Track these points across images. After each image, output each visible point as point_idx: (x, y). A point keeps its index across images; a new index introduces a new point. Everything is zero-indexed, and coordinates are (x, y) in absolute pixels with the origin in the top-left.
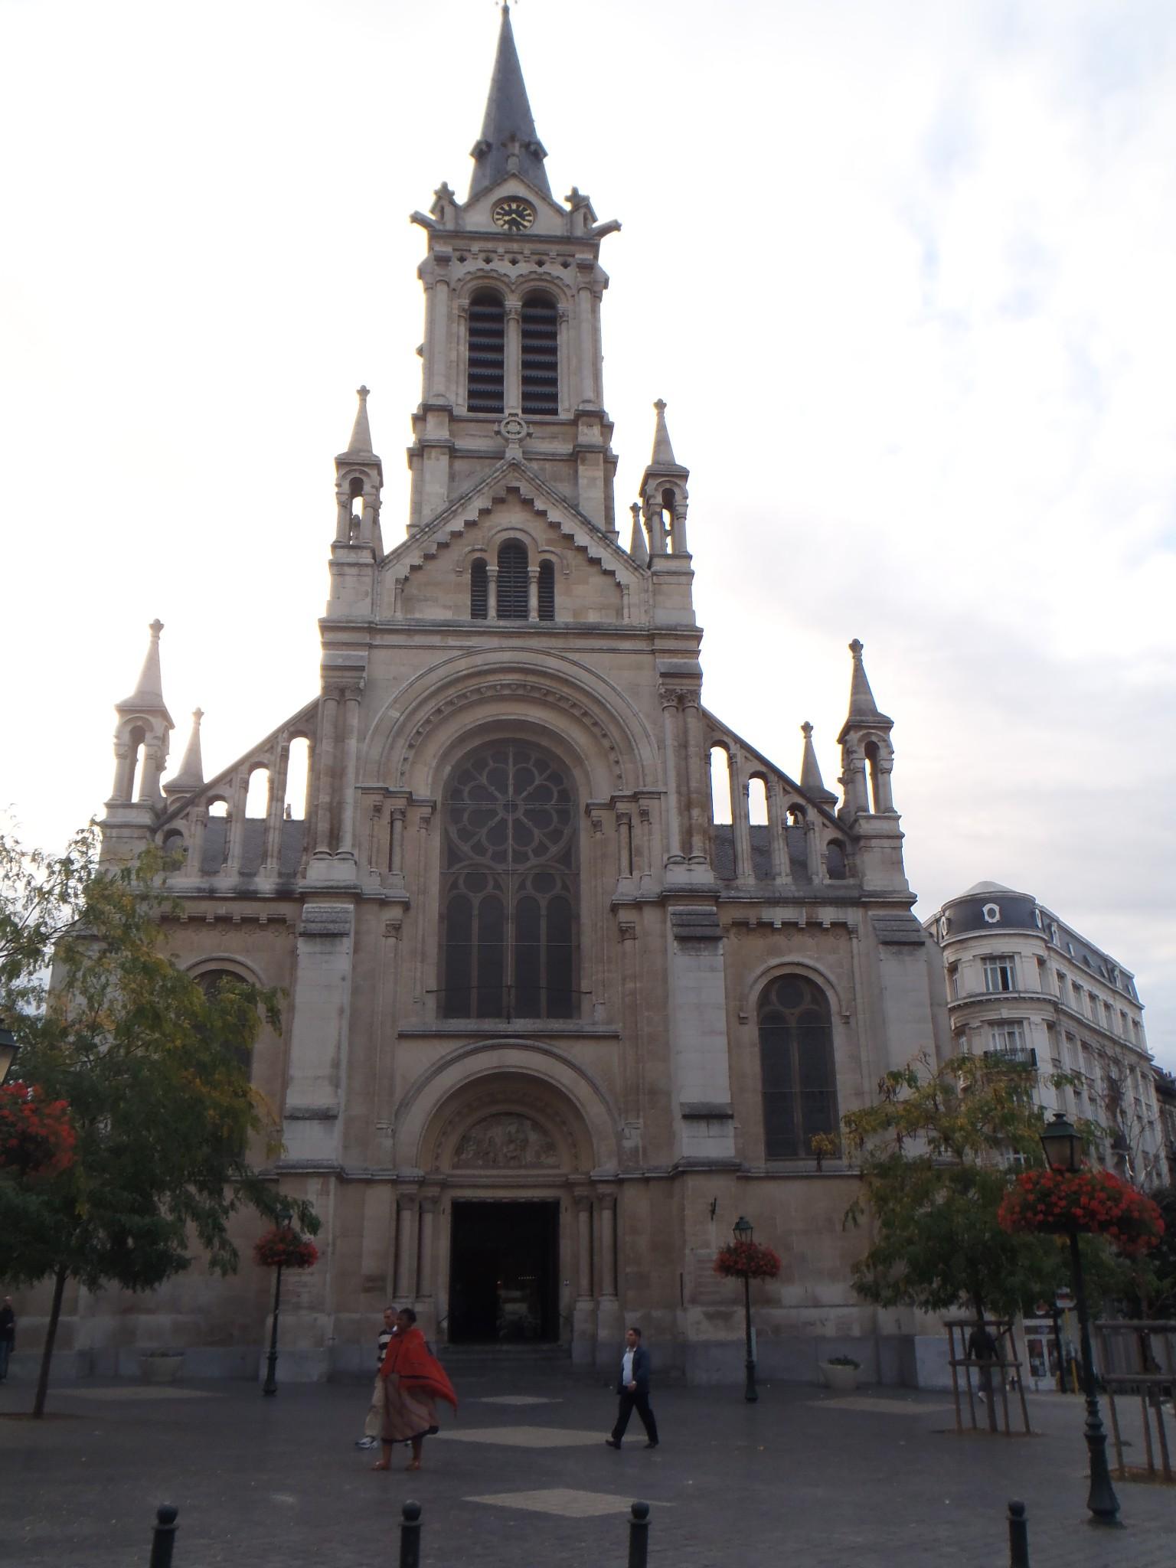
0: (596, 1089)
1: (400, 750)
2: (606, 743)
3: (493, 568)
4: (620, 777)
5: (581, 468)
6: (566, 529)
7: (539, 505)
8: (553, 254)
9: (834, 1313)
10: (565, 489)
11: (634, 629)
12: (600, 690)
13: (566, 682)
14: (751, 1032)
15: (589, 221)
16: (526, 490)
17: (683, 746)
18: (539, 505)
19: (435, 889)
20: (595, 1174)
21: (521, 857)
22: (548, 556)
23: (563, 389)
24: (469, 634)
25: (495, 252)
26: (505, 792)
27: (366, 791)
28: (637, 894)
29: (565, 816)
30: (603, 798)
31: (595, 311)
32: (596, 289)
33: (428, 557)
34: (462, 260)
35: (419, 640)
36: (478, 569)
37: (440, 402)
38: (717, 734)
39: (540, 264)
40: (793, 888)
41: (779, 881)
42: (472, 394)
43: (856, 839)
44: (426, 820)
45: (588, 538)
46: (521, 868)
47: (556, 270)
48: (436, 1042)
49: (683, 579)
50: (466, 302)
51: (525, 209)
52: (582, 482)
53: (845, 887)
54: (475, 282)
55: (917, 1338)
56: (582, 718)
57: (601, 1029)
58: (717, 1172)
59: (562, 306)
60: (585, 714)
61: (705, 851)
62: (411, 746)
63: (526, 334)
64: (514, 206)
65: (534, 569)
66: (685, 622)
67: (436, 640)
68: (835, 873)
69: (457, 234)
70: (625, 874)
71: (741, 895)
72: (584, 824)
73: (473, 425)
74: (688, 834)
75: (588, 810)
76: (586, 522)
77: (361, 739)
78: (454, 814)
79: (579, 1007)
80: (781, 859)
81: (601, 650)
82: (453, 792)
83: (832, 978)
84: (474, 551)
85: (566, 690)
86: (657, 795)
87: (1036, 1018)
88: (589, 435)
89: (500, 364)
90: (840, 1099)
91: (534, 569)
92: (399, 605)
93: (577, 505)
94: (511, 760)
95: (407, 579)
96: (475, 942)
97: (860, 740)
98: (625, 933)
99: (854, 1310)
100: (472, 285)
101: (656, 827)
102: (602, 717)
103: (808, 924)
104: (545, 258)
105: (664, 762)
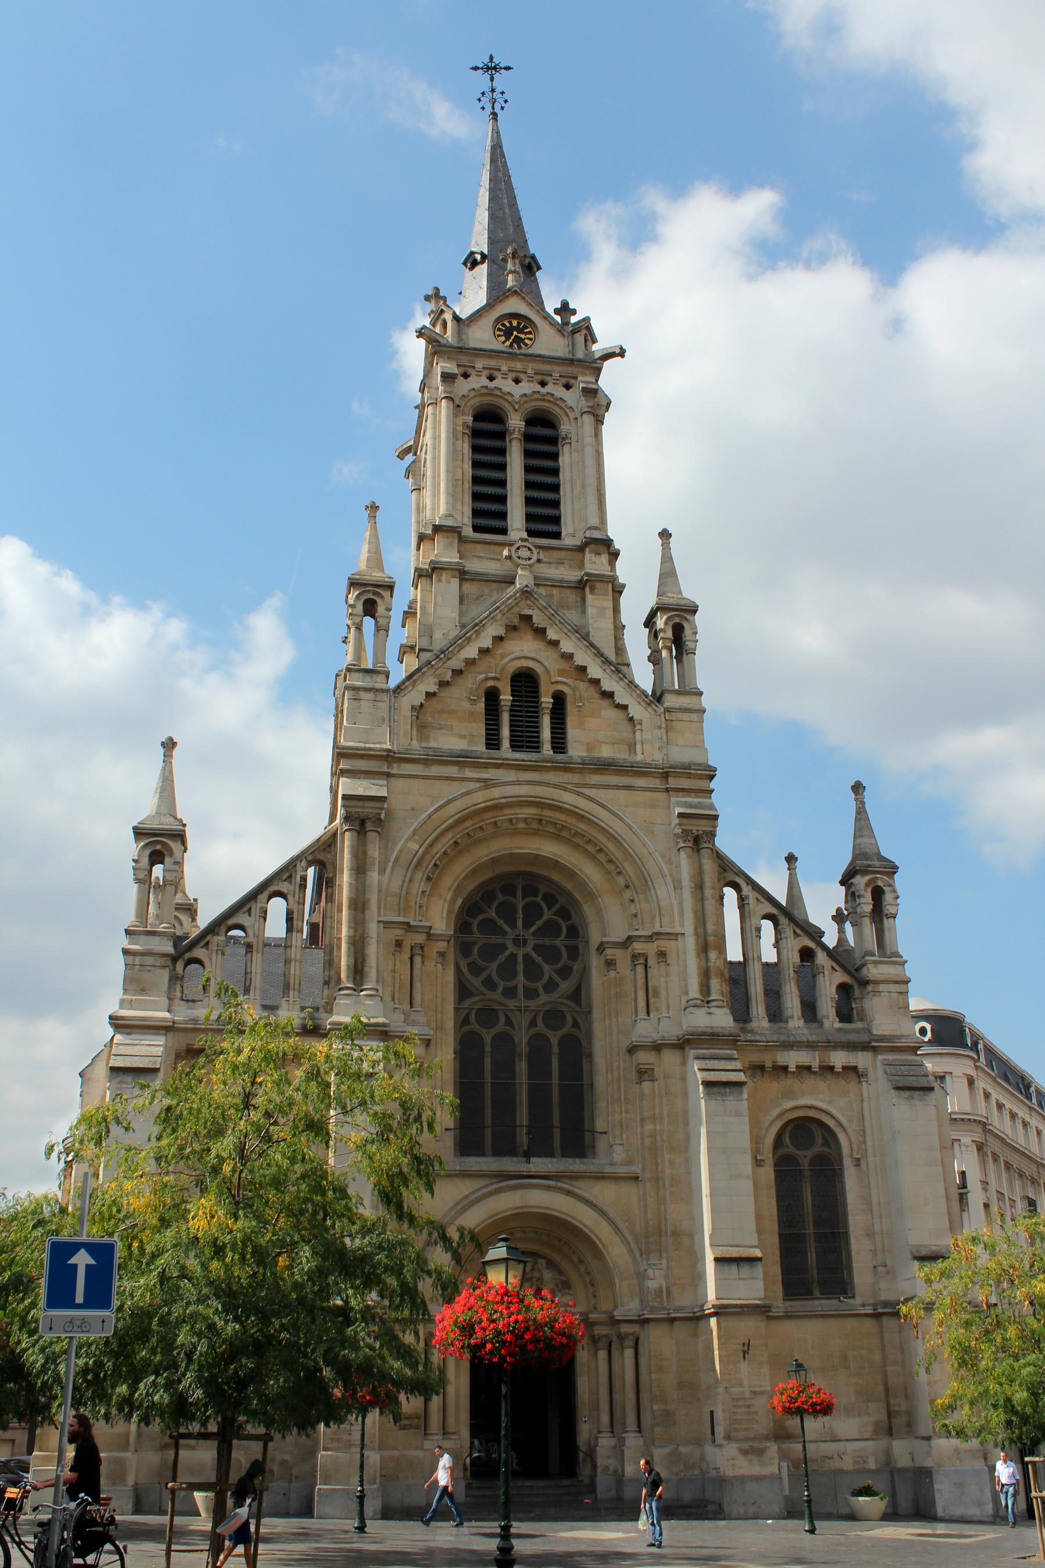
1: (419, 885)
2: (621, 881)
3: (506, 697)
4: (635, 916)
5: (589, 597)
7: (552, 634)
8: (556, 375)
9: (851, 1447)
10: (573, 616)
11: (648, 765)
12: (616, 827)
14: (768, 1173)
15: (589, 343)
16: (538, 619)
17: (699, 887)
18: (552, 634)
19: (450, 1025)
20: (618, 1314)
21: (531, 994)
22: (560, 687)
24: (486, 766)
25: (499, 370)
26: (513, 926)
27: (387, 924)
28: (656, 1036)
29: (574, 952)
30: (618, 934)
31: (597, 435)
33: (443, 684)
35: (436, 770)
36: (492, 697)
37: (449, 523)
38: (730, 874)
39: (543, 384)
40: (806, 1032)
42: (476, 513)
43: (864, 983)
44: (442, 955)
46: (533, 1004)
47: (560, 392)
49: (694, 717)
50: (469, 419)
51: (525, 327)
52: (590, 611)
53: (855, 1031)
54: (478, 399)
56: (597, 854)
57: (621, 1170)
59: (565, 428)
62: (429, 879)
63: (528, 454)
65: (546, 700)
66: (697, 760)
67: (453, 771)
68: (845, 1015)
69: (460, 351)
70: (642, 1014)
71: (757, 1038)
72: (595, 962)
73: (479, 546)
74: (706, 975)
75: (601, 948)
76: (599, 654)
77: (382, 871)
78: (464, 949)
79: (593, 1147)
81: (617, 787)
82: (463, 926)
83: (844, 1121)
84: (487, 679)
85: (582, 826)
86: (674, 936)
87: (966, 1140)
88: (595, 563)
89: (503, 483)
90: (853, 1240)
91: (546, 700)
94: (520, 894)
95: (422, 705)
97: (867, 885)
98: (644, 1074)
101: (674, 969)
102: (618, 855)
103: (820, 1067)
104: (547, 378)
105: (681, 903)
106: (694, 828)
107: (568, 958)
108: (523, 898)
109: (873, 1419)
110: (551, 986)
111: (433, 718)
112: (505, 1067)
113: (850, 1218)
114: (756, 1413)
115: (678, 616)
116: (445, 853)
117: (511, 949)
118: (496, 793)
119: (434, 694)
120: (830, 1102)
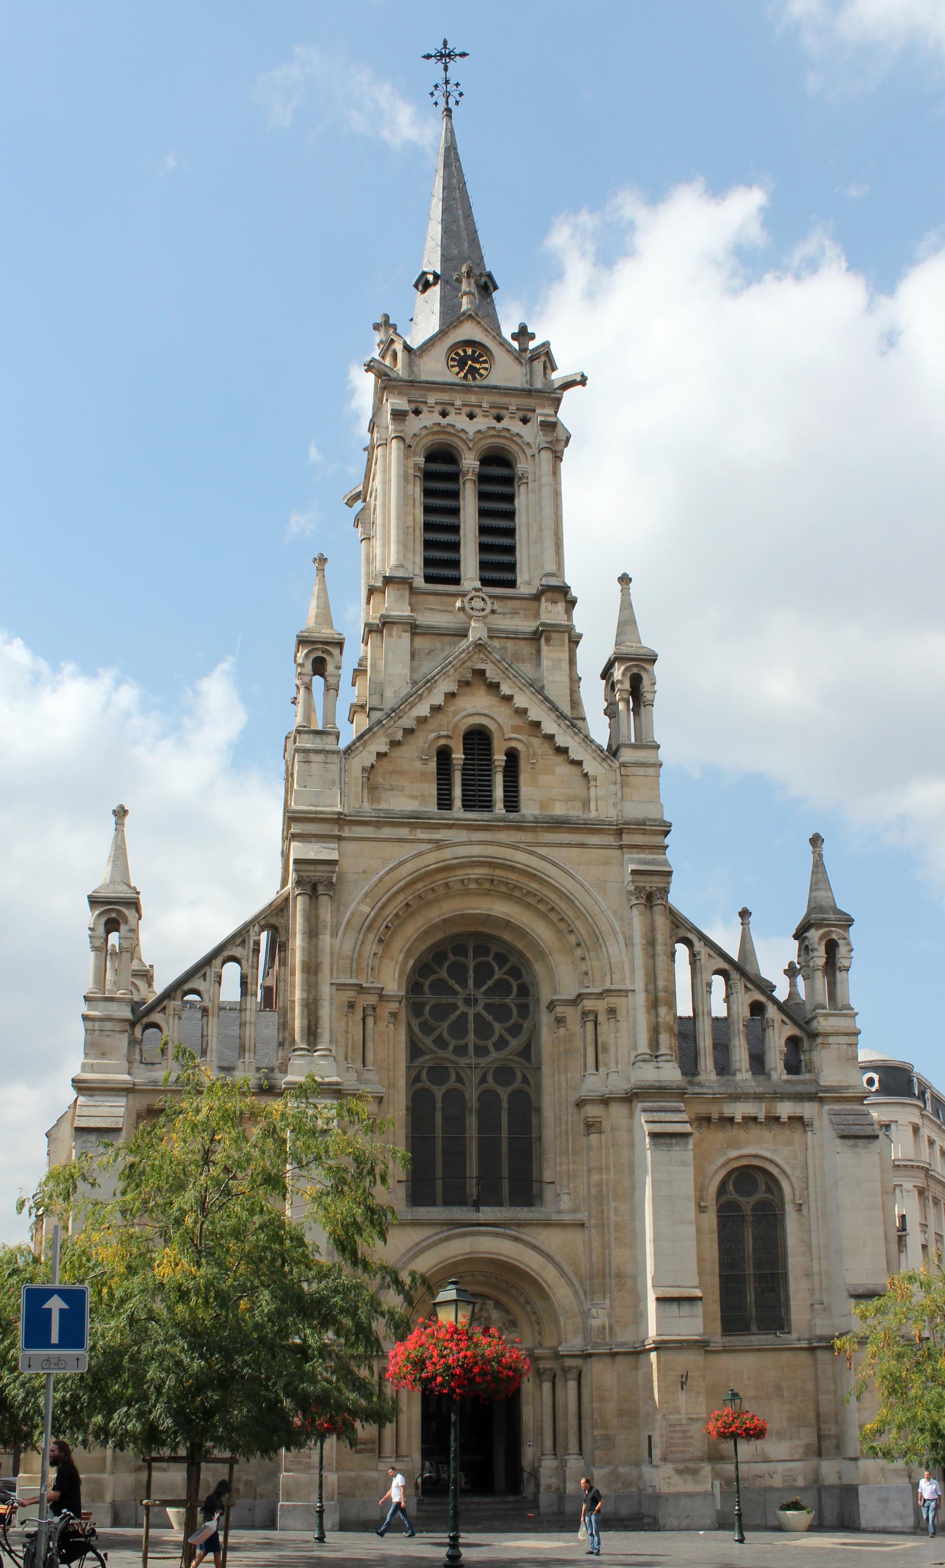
0: (563, 1273)
1: (372, 946)
2: (572, 939)
3: (458, 756)
4: (586, 973)
5: (544, 648)
6: (533, 715)
7: (505, 689)
8: (513, 408)
9: (780, 1467)
10: (527, 669)
11: (602, 822)
12: (568, 885)
13: (534, 877)
14: (711, 1219)
15: (549, 371)
16: (492, 674)
17: (651, 943)
18: (505, 689)
19: (402, 1083)
20: (562, 1350)
21: (481, 1051)
22: (514, 744)
23: (522, 557)
25: (453, 404)
27: (340, 987)
28: (604, 1091)
29: (524, 1010)
31: (556, 472)
32: (559, 448)
33: (394, 744)
34: (417, 412)
35: (387, 832)
36: (444, 755)
37: (400, 573)
39: (499, 418)
40: (753, 1084)
41: (739, 1077)
42: (428, 562)
43: (813, 1036)
44: (394, 1015)
45: (555, 725)
46: (483, 1061)
47: (516, 426)
48: (410, 1230)
49: (651, 771)
50: (421, 460)
51: (481, 356)
52: (545, 663)
53: (803, 1082)
54: (430, 438)
55: (860, 1488)
56: (548, 913)
57: (568, 1217)
58: (688, 1348)
59: (522, 466)
60: (552, 909)
61: (671, 1048)
62: (380, 941)
64: (469, 352)
65: (499, 758)
66: (653, 816)
67: (404, 832)
68: (793, 1067)
70: (591, 1069)
71: (705, 1091)
72: (545, 1019)
73: (431, 598)
74: (655, 1030)
76: (554, 708)
77: (334, 935)
79: (541, 1196)
80: (740, 1054)
81: (570, 845)
82: (414, 987)
84: (439, 737)
86: (624, 993)
88: (552, 613)
89: (455, 529)
91: (499, 758)
92: (366, 794)
93: (543, 688)
94: (471, 954)
95: (373, 766)
96: (439, 1132)
97: (821, 939)
98: (591, 1126)
99: (799, 1464)
100: (427, 441)
101: (623, 1025)
103: (767, 1118)
104: (504, 412)
105: (632, 960)
106: (648, 885)
107: (518, 1016)
108: (474, 958)
109: (803, 1442)
110: (501, 1044)
111: (385, 779)
112: (455, 1122)
113: (790, 1259)
114: (692, 1437)
115: (636, 666)
116: (397, 915)
117: (462, 1008)
118: (447, 853)
119: (385, 754)
120: (775, 1151)
